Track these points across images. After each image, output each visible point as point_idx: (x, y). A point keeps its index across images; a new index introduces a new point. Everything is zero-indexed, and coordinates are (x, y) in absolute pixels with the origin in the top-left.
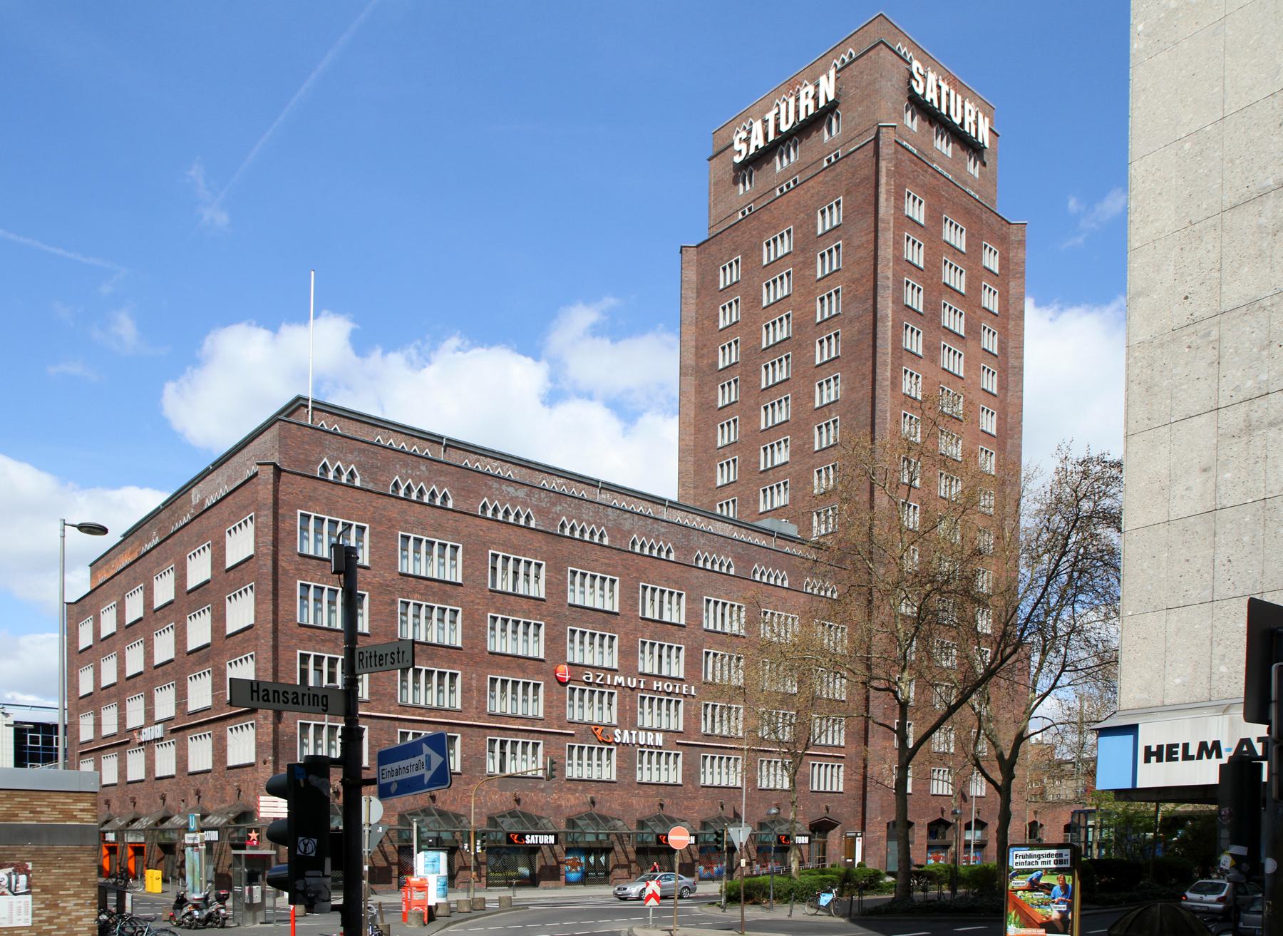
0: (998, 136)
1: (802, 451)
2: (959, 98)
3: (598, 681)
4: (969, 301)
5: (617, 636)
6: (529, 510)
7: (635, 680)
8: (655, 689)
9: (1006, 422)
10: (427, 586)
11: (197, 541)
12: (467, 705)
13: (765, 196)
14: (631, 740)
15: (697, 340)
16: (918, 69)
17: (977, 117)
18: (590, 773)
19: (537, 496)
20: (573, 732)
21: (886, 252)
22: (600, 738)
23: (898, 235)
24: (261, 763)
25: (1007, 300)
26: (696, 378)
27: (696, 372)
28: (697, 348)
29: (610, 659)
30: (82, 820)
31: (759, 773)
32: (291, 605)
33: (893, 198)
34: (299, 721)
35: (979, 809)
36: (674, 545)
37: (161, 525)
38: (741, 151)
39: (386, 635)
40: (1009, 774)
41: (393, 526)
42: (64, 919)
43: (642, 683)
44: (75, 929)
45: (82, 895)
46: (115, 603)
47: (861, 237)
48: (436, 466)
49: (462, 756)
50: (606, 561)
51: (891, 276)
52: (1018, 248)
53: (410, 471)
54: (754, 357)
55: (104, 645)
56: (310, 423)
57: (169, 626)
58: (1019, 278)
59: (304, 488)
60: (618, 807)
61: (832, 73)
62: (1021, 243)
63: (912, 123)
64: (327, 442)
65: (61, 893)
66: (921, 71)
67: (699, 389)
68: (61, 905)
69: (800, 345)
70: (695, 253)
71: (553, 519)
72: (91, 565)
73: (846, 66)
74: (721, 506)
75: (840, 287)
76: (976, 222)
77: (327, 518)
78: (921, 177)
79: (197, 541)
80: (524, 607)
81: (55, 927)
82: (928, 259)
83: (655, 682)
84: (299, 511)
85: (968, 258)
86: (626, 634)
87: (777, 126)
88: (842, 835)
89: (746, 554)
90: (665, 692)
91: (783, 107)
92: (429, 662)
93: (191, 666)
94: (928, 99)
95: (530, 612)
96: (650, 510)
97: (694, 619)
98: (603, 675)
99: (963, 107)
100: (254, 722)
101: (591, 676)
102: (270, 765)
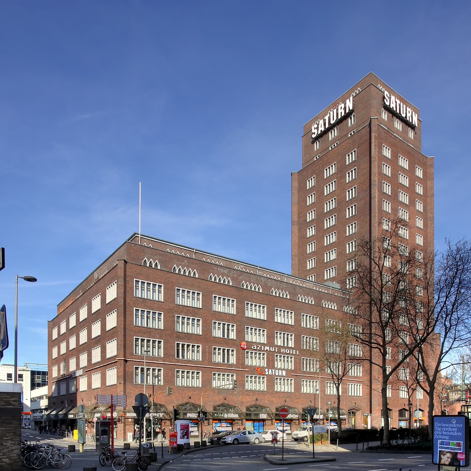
0: (421, 122)
1: (341, 253)
2: (404, 106)
3: (258, 349)
4: (410, 190)
5: (266, 330)
6: (229, 278)
7: (273, 348)
8: (282, 352)
9: (427, 241)
10: (187, 310)
11: (96, 293)
12: (204, 359)
13: (325, 151)
14: (272, 373)
15: (298, 211)
16: (387, 95)
17: (412, 114)
18: (259, 388)
19: (232, 272)
20: (248, 370)
21: (375, 170)
22: (259, 373)
23: (380, 163)
24: (118, 383)
25: (426, 189)
26: (298, 226)
27: (298, 223)
28: (298, 214)
29: (263, 340)
30: (14, 405)
31: (326, 385)
32: (131, 318)
33: (377, 148)
34: (134, 366)
35: (420, 405)
36: (289, 292)
37: (83, 288)
38: (315, 132)
39: (170, 330)
40: (432, 387)
41: (173, 285)
42: (6, 450)
43: (276, 349)
44: (11, 455)
45: (14, 440)
46: (65, 320)
47: (364, 165)
48: (191, 260)
49: (202, 381)
50: (261, 299)
51: (377, 180)
52: (430, 168)
53: (180, 263)
54: (321, 217)
55: (63, 338)
56: (140, 243)
57: (85, 328)
58: (431, 180)
59: (137, 270)
60: (267, 402)
61: (351, 98)
62: (432, 166)
63: (385, 116)
64: (146, 251)
65: (4, 438)
66: (388, 95)
67: (300, 230)
68: (4, 444)
69: (340, 211)
70: (297, 175)
71: (239, 282)
72: (57, 306)
73: (357, 95)
74: (309, 277)
75: (356, 186)
76: (412, 157)
77: (146, 282)
78: (389, 139)
79: (96, 293)
80: (228, 318)
81: (1, 454)
82: (392, 173)
83: (282, 349)
84: (135, 279)
85: (410, 172)
86: (270, 329)
87: (329, 121)
88: (362, 415)
89: (319, 297)
90: (286, 353)
91: (332, 113)
92: (188, 341)
93: (93, 345)
94: (391, 107)
95: (230, 320)
96: (279, 278)
97: (298, 323)
98: (260, 346)
99: (406, 110)
100: (116, 367)
101: (255, 346)
102: (122, 385)
